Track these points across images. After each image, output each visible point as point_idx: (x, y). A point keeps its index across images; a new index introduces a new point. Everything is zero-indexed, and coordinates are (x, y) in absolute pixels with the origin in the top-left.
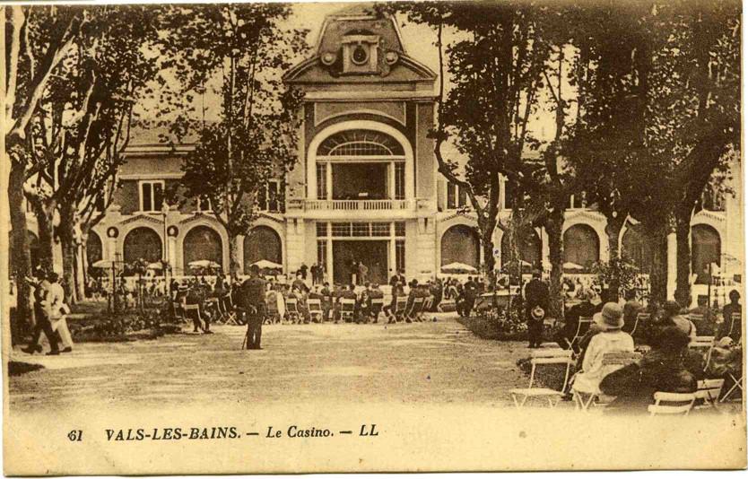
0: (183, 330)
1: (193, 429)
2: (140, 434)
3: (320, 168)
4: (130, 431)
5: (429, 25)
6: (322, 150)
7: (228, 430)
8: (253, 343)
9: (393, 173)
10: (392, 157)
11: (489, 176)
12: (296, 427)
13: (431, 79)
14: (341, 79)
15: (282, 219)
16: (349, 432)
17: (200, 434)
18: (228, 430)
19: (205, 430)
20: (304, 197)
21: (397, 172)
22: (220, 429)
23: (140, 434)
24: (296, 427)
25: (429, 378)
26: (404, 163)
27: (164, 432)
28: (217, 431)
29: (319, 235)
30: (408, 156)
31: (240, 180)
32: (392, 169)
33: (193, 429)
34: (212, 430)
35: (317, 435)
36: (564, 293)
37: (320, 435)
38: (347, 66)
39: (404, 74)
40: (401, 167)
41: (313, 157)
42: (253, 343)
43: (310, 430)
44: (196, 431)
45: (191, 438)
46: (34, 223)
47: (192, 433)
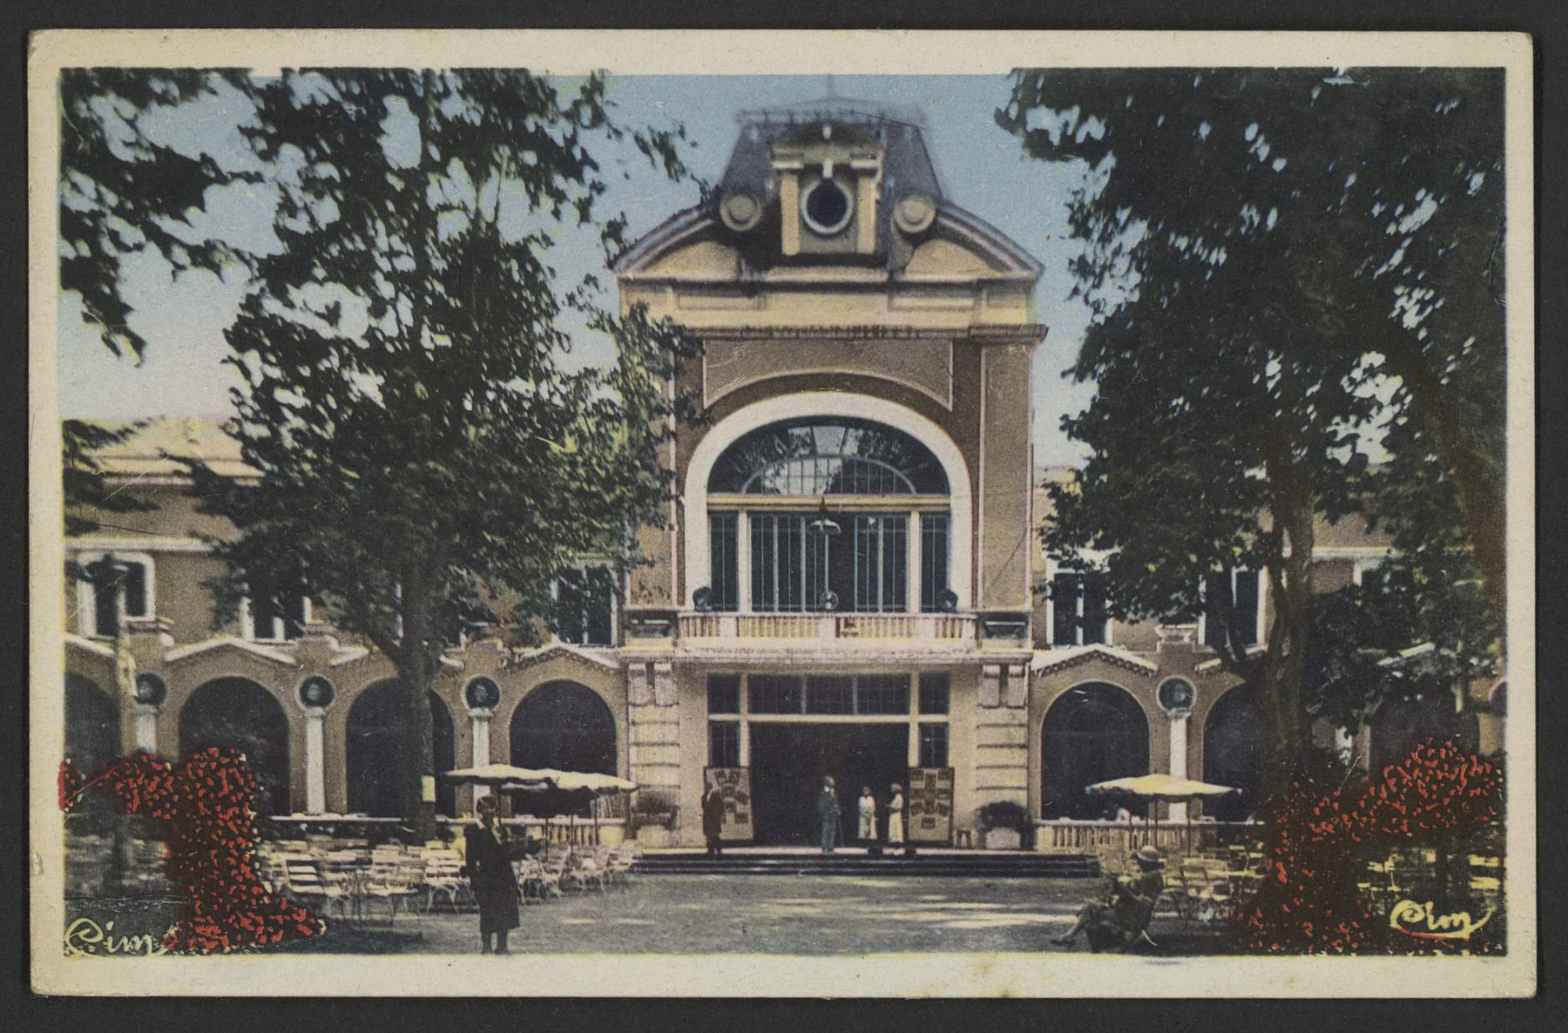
0: (490, 219)
3: (722, 525)
5: (1083, 413)
6: (726, 474)
9: (904, 501)
10: (911, 503)
13: (1025, 274)
14: (772, 276)
20: (675, 607)
21: (926, 539)
26: (948, 514)
29: (713, 709)
30: (959, 501)
31: (496, 820)
32: (914, 525)
35: (702, 635)
36: (1355, 713)
38: (791, 243)
39: (944, 263)
40: (937, 526)
41: (696, 499)
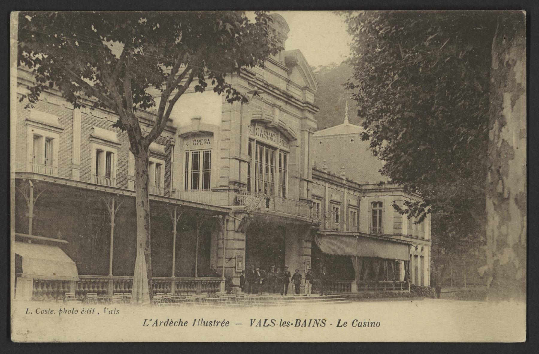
1: (297, 320)
2: (273, 323)
4: (266, 320)
7: (321, 321)
8: (394, 202)
11: (54, 47)
12: (357, 321)
15: (295, 70)
16: (193, 325)
17: (301, 324)
18: (321, 321)
19: (305, 321)
22: (316, 320)
23: (273, 323)
24: (357, 321)
25: (321, 143)
27: (295, 321)
28: (313, 322)
33: (297, 320)
34: (264, 321)
37: (182, 325)
42: (394, 202)
43: (213, 321)
44: (299, 321)
45: (296, 326)
46: (243, 240)
47: (296, 323)
